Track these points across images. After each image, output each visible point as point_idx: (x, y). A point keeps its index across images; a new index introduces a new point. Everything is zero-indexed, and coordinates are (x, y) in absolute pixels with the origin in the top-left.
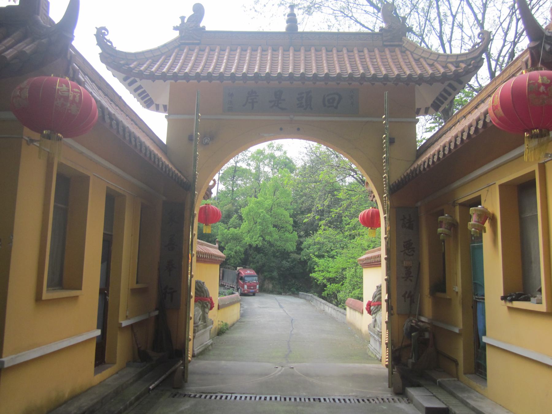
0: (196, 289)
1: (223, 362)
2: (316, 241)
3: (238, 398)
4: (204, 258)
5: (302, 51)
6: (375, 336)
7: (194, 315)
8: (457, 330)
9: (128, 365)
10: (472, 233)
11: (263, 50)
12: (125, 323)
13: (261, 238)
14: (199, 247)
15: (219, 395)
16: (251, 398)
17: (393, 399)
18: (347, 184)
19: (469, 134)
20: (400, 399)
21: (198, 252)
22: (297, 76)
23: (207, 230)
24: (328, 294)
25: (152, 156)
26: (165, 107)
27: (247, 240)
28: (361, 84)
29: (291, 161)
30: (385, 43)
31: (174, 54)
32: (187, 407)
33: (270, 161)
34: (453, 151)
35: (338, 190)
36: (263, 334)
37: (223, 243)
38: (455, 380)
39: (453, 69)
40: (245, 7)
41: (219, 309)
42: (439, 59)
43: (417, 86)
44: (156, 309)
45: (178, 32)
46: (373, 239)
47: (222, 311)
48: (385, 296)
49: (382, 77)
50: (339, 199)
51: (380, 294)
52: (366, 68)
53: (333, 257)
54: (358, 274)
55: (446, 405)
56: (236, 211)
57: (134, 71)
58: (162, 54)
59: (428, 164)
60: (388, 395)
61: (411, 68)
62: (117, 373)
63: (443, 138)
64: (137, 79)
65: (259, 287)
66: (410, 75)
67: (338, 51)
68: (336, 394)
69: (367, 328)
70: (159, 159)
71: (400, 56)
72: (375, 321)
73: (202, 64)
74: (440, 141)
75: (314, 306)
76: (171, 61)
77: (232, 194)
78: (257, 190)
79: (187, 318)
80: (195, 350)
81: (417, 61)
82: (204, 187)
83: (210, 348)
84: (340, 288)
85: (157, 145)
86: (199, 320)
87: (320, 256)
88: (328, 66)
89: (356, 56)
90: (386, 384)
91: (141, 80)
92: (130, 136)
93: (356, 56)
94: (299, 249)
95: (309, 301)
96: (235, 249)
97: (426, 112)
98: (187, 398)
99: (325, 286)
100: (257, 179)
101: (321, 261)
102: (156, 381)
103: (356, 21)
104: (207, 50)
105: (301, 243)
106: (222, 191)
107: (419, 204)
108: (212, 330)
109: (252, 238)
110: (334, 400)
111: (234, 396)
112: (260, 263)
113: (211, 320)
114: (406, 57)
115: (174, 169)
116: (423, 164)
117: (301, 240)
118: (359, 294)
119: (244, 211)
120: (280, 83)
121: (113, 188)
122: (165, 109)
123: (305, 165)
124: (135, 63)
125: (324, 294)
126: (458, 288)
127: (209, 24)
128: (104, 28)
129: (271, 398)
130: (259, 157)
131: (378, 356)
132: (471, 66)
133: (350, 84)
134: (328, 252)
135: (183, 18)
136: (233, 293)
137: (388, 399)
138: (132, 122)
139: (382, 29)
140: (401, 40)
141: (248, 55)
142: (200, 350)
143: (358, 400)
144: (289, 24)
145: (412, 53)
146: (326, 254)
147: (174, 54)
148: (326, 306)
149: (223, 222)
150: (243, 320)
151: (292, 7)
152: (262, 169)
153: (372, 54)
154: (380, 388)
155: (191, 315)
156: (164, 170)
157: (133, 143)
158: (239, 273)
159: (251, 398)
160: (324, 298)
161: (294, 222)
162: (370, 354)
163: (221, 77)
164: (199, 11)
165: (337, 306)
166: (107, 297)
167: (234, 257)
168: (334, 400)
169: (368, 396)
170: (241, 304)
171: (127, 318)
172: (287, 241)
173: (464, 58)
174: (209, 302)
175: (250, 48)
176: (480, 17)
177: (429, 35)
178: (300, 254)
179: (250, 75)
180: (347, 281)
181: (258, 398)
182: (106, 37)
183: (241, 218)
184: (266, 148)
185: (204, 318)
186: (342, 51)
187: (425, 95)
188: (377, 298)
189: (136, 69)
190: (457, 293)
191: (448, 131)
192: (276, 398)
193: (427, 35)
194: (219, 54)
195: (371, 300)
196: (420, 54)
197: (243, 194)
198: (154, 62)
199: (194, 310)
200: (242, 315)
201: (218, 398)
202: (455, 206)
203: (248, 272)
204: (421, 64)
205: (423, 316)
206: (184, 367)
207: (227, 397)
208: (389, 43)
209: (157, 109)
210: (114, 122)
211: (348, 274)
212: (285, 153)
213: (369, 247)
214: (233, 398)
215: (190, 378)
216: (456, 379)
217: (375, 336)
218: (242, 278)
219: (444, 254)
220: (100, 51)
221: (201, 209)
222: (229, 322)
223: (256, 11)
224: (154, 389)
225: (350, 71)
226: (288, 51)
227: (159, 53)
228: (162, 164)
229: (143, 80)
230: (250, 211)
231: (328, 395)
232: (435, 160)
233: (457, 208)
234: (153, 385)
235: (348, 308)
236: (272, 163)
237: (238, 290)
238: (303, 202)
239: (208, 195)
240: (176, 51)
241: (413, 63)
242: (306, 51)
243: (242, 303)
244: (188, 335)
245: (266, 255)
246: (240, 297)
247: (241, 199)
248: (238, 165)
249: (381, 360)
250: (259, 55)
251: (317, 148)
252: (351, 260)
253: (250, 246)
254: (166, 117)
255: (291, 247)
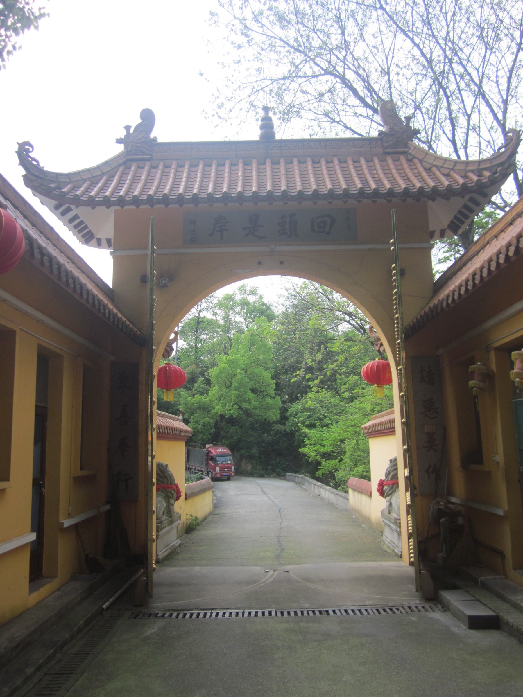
0: (158, 474)
1: (197, 568)
2: (307, 406)
3: (220, 615)
4: (168, 434)
5: (282, 163)
6: (392, 525)
7: (157, 508)
8: (501, 513)
9: (73, 577)
10: (516, 385)
11: (232, 165)
12: (67, 523)
13: (236, 406)
14: (161, 420)
15: (195, 613)
16: (237, 614)
17: (423, 607)
18: (340, 333)
19: (507, 256)
20: (433, 606)
21: (158, 426)
22: (278, 194)
23: (168, 397)
24: (323, 474)
25: (96, 302)
26: (109, 241)
27: (218, 408)
28: (360, 202)
29: (268, 308)
30: (386, 150)
31: (118, 173)
32: (153, 631)
33: (242, 309)
34: (486, 280)
35: (331, 340)
36: (250, 527)
37: (187, 414)
38: (501, 578)
39: (475, 178)
40: (206, 113)
41: (186, 499)
42: (456, 168)
43: (430, 202)
44: (107, 503)
45: (122, 145)
46: (379, 401)
47: (190, 501)
48: (403, 473)
49: (386, 191)
50: (332, 352)
51: (396, 469)
52: (365, 181)
53: (327, 426)
54: (361, 447)
55: (494, 611)
56: (202, 374)
57: (68, 196)
58: (104, 174)
59: (453, 298)
60: (416, 602)
61: (422, 180)
62: (59, 589)
63: (468, 265)
64: (73, 207)
65: (235, 469)
66: (421, 189)
67: (327, 162)
68: (348, 604)
69: (380, 515)
70: (105, 306)
71: (406, 166)
72: (391, 505)
73: (155, 184)
74: (464, 269)
75: (306, 490)
76: (115, 182)
77: (196, 352)
78: (227, 345)
79: (148, 512)
80: (159, 553)
81: (428, 170)
82: (163, 341)
83: (178, 550)
84: (337, 466)
85: (101, 290)
86: (163, 514)
87: (312, 426)
88: (316, 181)
89: (351, 167)
90: (413, 588)
91: (77, 207)
92: (67, 276)
93: (351, 167)
94: (283, 418)
95: (298, 483)
96: (202, 421)
97: (442, 235)
98: (152, 619)
99: (319, 464)
100: (227, 331)
101: (311, 432)
102: (111, 597)
103: (346, 127)
104: (160, 167)
105: (286, 410)
106: (182, 349)
107: (440, 351)
108: (180, 527)
109: (224, 406)
110: (346, 611)
111: (214, 612)
112: (235, 438)
113: (178, 513)
114: (414, 167)
115: (124, 319)
116: (445, 298)
117: (286, 406)
118: (363, 471)
119: (213, 373)
120: (256, 204)
121: (46, 345)
122: (109, 243)
123: (287, 311)
124: (69, 186)
125: (319, 473)
126: (500, 458)
127: (163, 133)
128: (28, 144)
129: (263, 613)
130: (228, 303)
131: (396, 550)
132: (498, 174)
133: (345, 202)
134: (321, 420)
135: (128, 128)
136: (202, 478)
137: (416, 607)
138: (69, 260)
139: (381, 133)
140: (406, 146)
141: (213, 170)
142: (166, 554)
143: (378, 610)
144: (263, 130)
145: (421, 161)
146: (318, 423)
147: (118, 173)
148: (321, 490)
149: (186, 388)
150: (218, 512)
151: (266, 109)
152: (233, 319)
153: (371, 164)
154: (404, 593)
155: (154, 508)
156: (112, 320)
157: (72, 286)
158: (209, 452)
159: (237, 614)
160: (318, 479)
161: (277, 384)
162: (385, 548)
163: (180, 199)
164: (148, 118)
165: (336, 488)
166: (43, 490)
167: (202, 432)
168: (346, 611)
169: (390, 605)
170: (213, 492)
171: (69, 516)
172: (268, 408)
173: (488, 165)
174: (174, 490)
175: (215, 162)
176: (500, 116)
177: (437, 142)
178: (284, 424)
179: (218, 196)
180: (347, 455)
181: (246, 614)
182: (30, 154)
183: (208, 382)
184: (237, 292)
185: (169, 512)
186: (332, 162)
187: (440, 214)
188: (391, 475)
189: (70, 194)
190: (498, 463)
191: (474, 256)
192: (270, 613)
193: (434, 142)
194: (176, 171)
195: (383, 478)
196: (431, 162)
197: (209, 352)
198: (93, 184)
199: (157, 502)
200: (215, 506)
201: (194, 616)
202: (489, 352)
203: (219, 450)
204: (434, 175)
205: (453, 495)
206: (147, 577)
207: (205, 614)
208: (391, 150)
209: (99, 244)
210: (46, 258)
211: (348, 446)
212: (261, 297)
213: (373, 410)
214: (214, 615)
215: (156, 591)
216: (503, 576)
217: (392, 525)
218: (212, 459)
219: (477, 415)
220: (24, 172)
221: (160, 370)
222: (200, 515)
223: (219, 117)
224: (108, 608)
225: (344, 186)
226: (264, 164)
227: (100, 173)
228: (109, 312)
229: (80, 208)
230: (221, 372)
231: (338, 606)
232: (462, 292)
233: (492, 354)
234: (107, 603)
235: (350, 491)
236: (245, 311)
237: (208, 474)
238: (286, 358)
239: (168, 350)
240: (121, 169)
241: (424, 174)
242: (286, 163)
243: (213, 490)
244: (151, 535)
245: (241, 427)
246: (212, 483)
247: (207, 358)
248: (202, 315)
249: (401, 556)
250: (227, 170)
251: (306, 287)
252: (351, 429)
253: (222, 416)
254: (111, 253)
255: (273, 415)
